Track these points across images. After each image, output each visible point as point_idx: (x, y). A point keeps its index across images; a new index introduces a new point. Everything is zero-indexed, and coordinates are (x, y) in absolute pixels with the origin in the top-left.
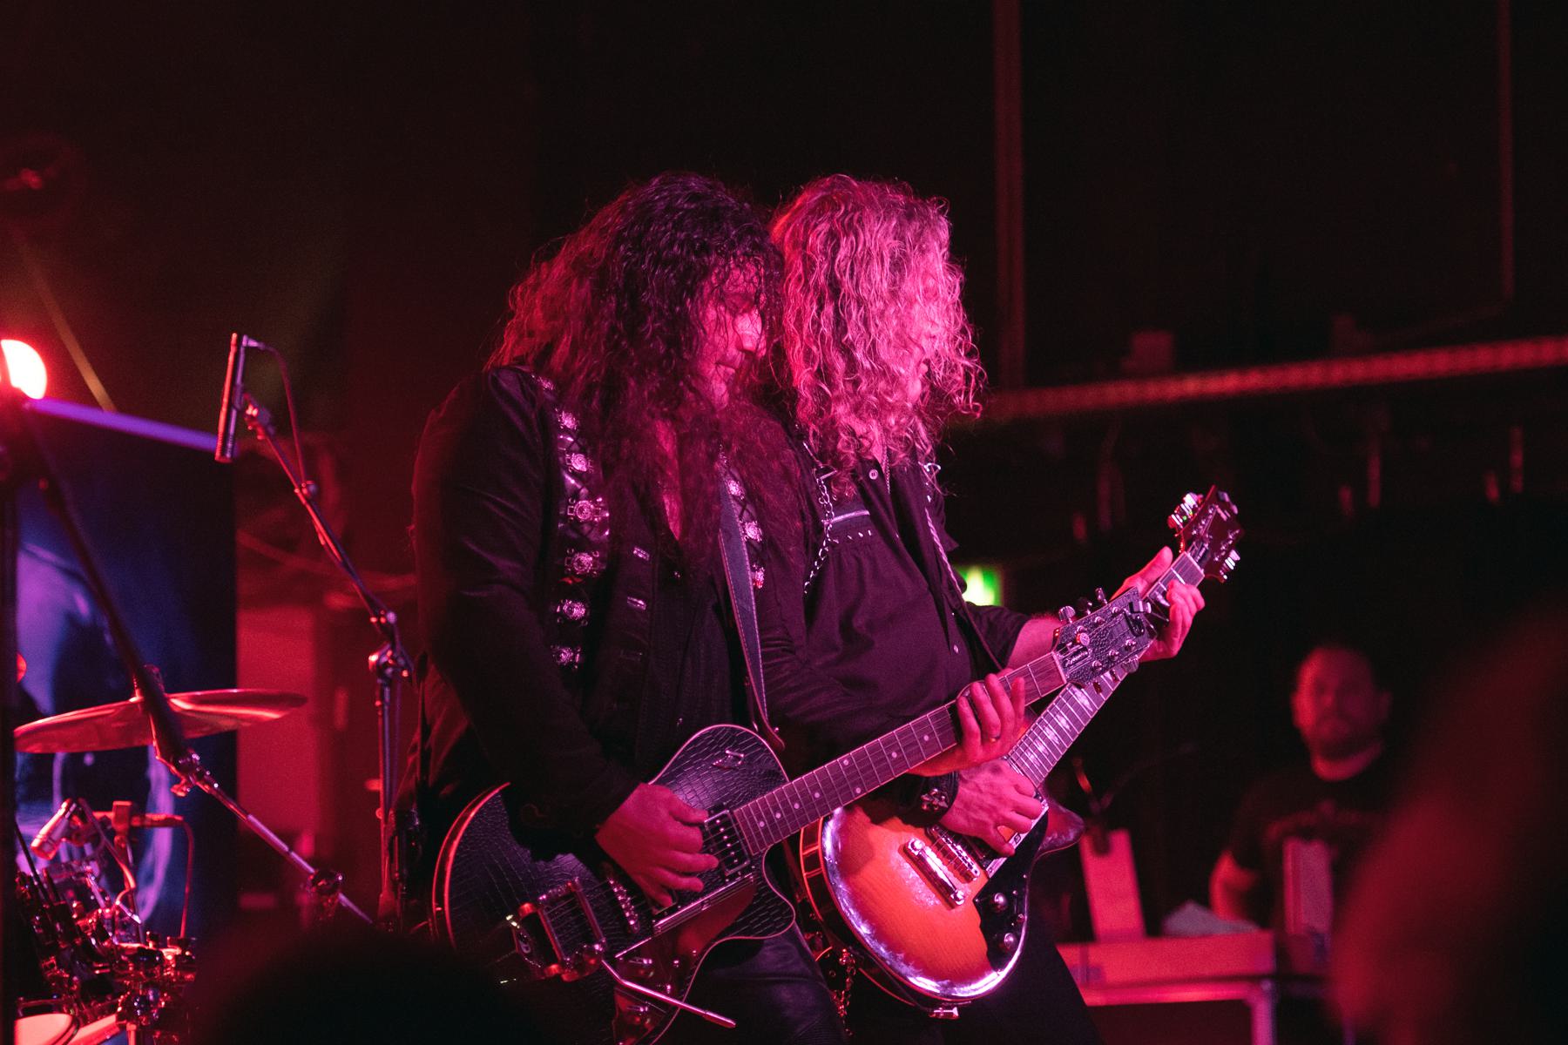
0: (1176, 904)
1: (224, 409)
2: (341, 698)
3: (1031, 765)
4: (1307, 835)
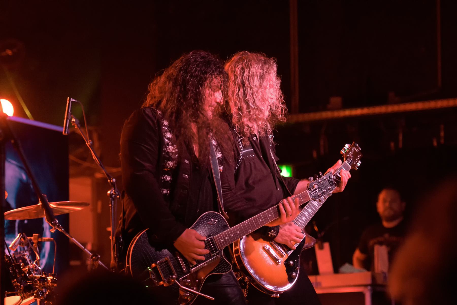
1: (65, 119)
2: (100, 204)
4: (381, 243)
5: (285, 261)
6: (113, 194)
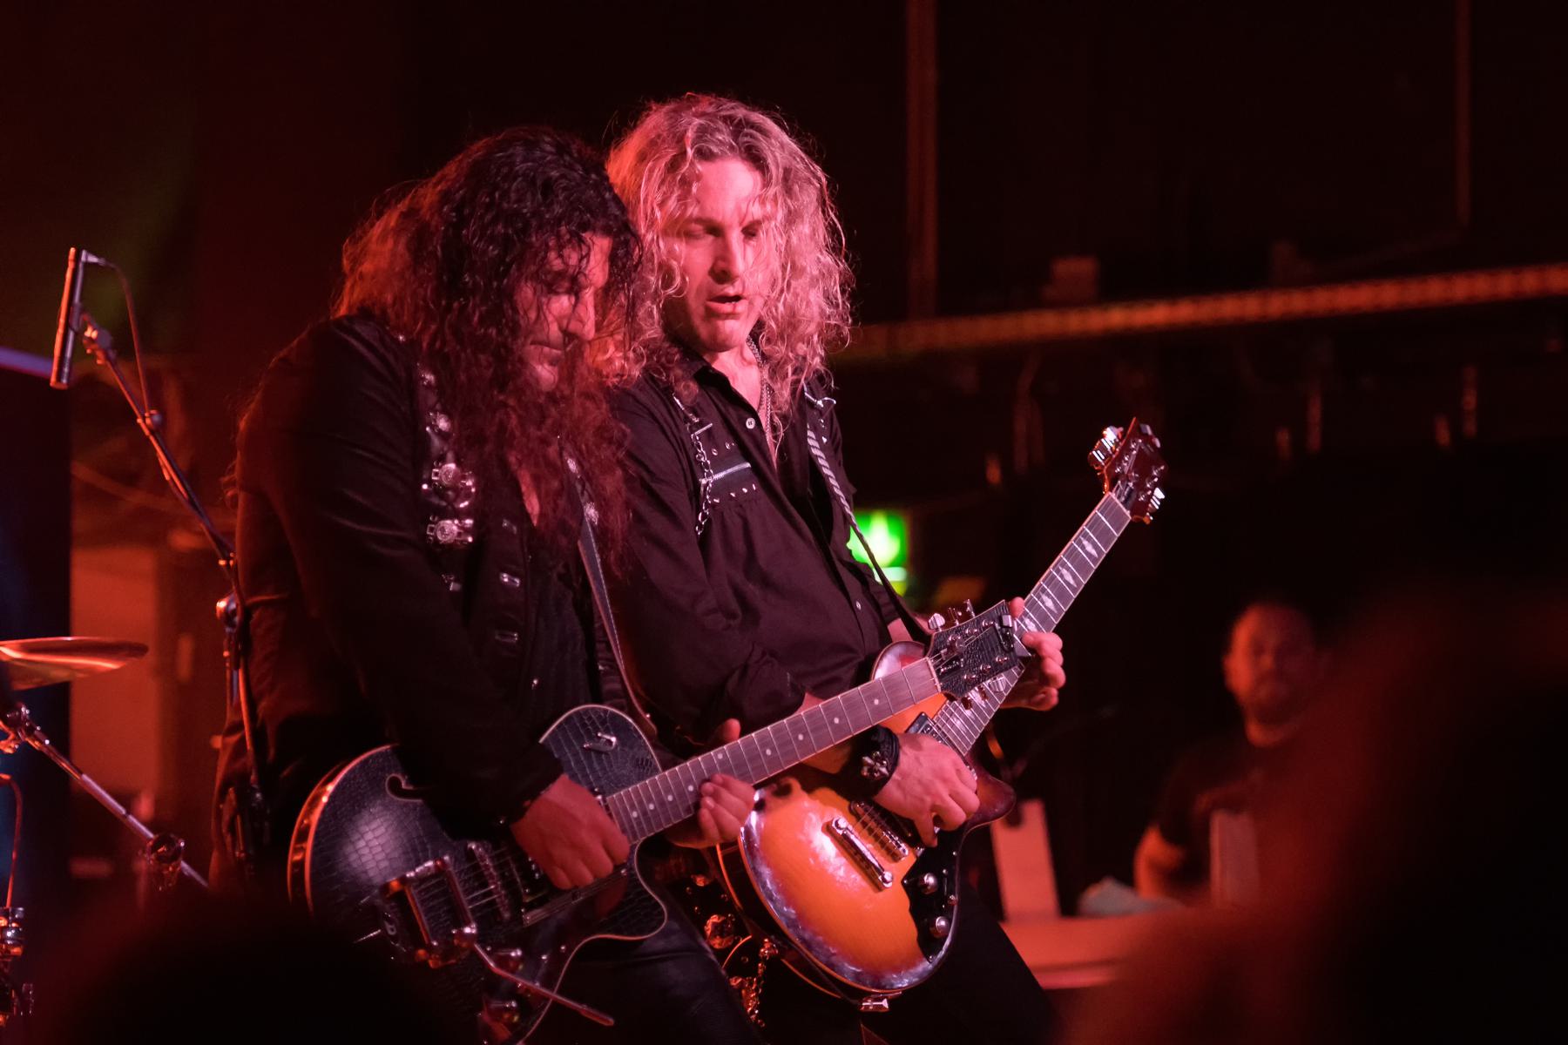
0: (1095, 879)
1: (60, 331)
2: (186, 646)
3: (958, 732)
4: (1233, 806)
5: (907, 876)
6: (234, 612)
